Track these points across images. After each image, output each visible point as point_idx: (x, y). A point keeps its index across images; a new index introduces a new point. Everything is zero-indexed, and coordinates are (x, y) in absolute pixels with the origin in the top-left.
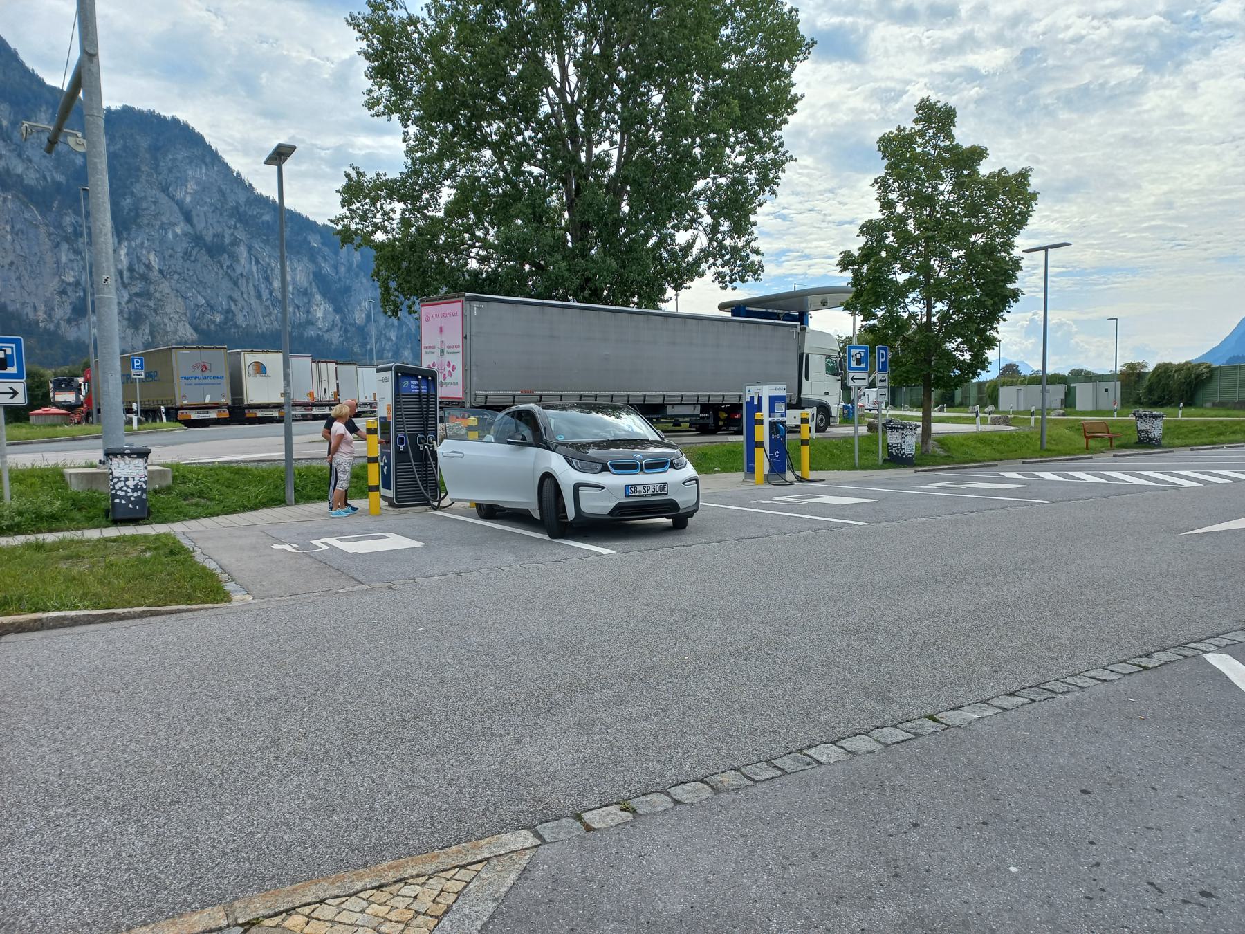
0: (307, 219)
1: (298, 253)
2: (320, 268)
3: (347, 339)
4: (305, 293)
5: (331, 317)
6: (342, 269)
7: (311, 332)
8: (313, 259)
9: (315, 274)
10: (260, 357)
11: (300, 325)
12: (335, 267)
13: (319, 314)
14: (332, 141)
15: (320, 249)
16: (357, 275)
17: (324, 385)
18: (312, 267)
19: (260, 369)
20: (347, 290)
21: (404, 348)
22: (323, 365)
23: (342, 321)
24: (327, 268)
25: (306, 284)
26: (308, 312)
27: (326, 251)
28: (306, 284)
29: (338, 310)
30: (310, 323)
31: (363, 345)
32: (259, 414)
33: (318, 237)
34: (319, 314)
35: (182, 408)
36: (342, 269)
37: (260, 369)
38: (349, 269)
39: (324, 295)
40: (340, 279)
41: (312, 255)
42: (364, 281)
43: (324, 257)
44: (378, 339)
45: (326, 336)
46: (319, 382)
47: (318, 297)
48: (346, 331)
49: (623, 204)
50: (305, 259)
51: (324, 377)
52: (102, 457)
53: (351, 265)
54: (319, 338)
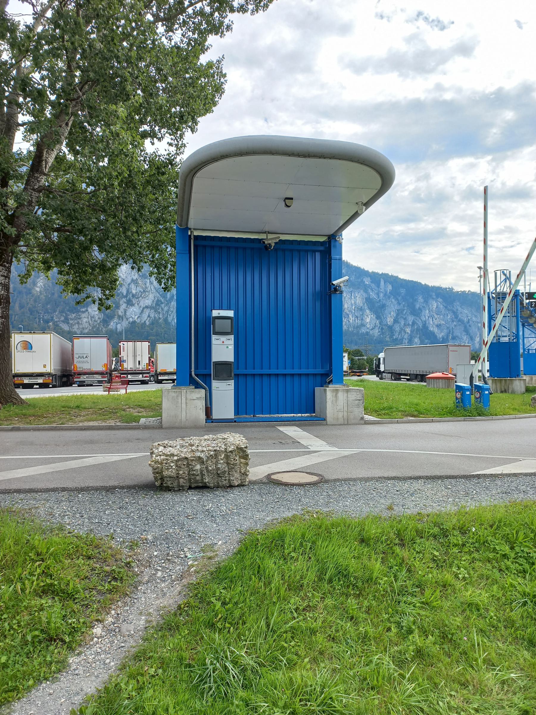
0: (364, 270)
1: (358, 288)
2: (369, 295)
3: (383, 333)
4: (361, 309)
5: (374, 322)
6: (381, 295)
7: (363, 330)
8: (366, 291)
9: (366, 298)
10: (27, 337)
11: (358, 327)
12: (378, 294)
13: (368, 320)
14: (382, 230)
15: (370, 285)
16: (389, 297)
17: (139, 358)
18: (365, 295)
19: (28, 346)
20: (383, 306)
21: (415, 337)
22: (138, 344)
23: (380, 323)
24: (373, 295)
25: (361, 305)
26: (362, 319)
27: (373, 285)
28: (361, 305)
29: (378, 317)
30: (363, 325)
31: (391, 337)
32: (26, 381)
33: (369, 279)
34: (368, 320)
35: (80, 374)
36: (381, 295)
37: (28, 346)
38: (385, 295)
39: (371, 310)
40: (380, 301)
41: (366, 289)
42: (393, 300)
43: (372, 289)
44: (400, 332)
45: (371, 332)
46: (135, 356)
47: (368, 311)
48: (382, 329)
49: (19, 135)
50: (362, 291)
51: (138, 352)
52: (523, 390)
53: (386, 292)
54: (367, 333)
